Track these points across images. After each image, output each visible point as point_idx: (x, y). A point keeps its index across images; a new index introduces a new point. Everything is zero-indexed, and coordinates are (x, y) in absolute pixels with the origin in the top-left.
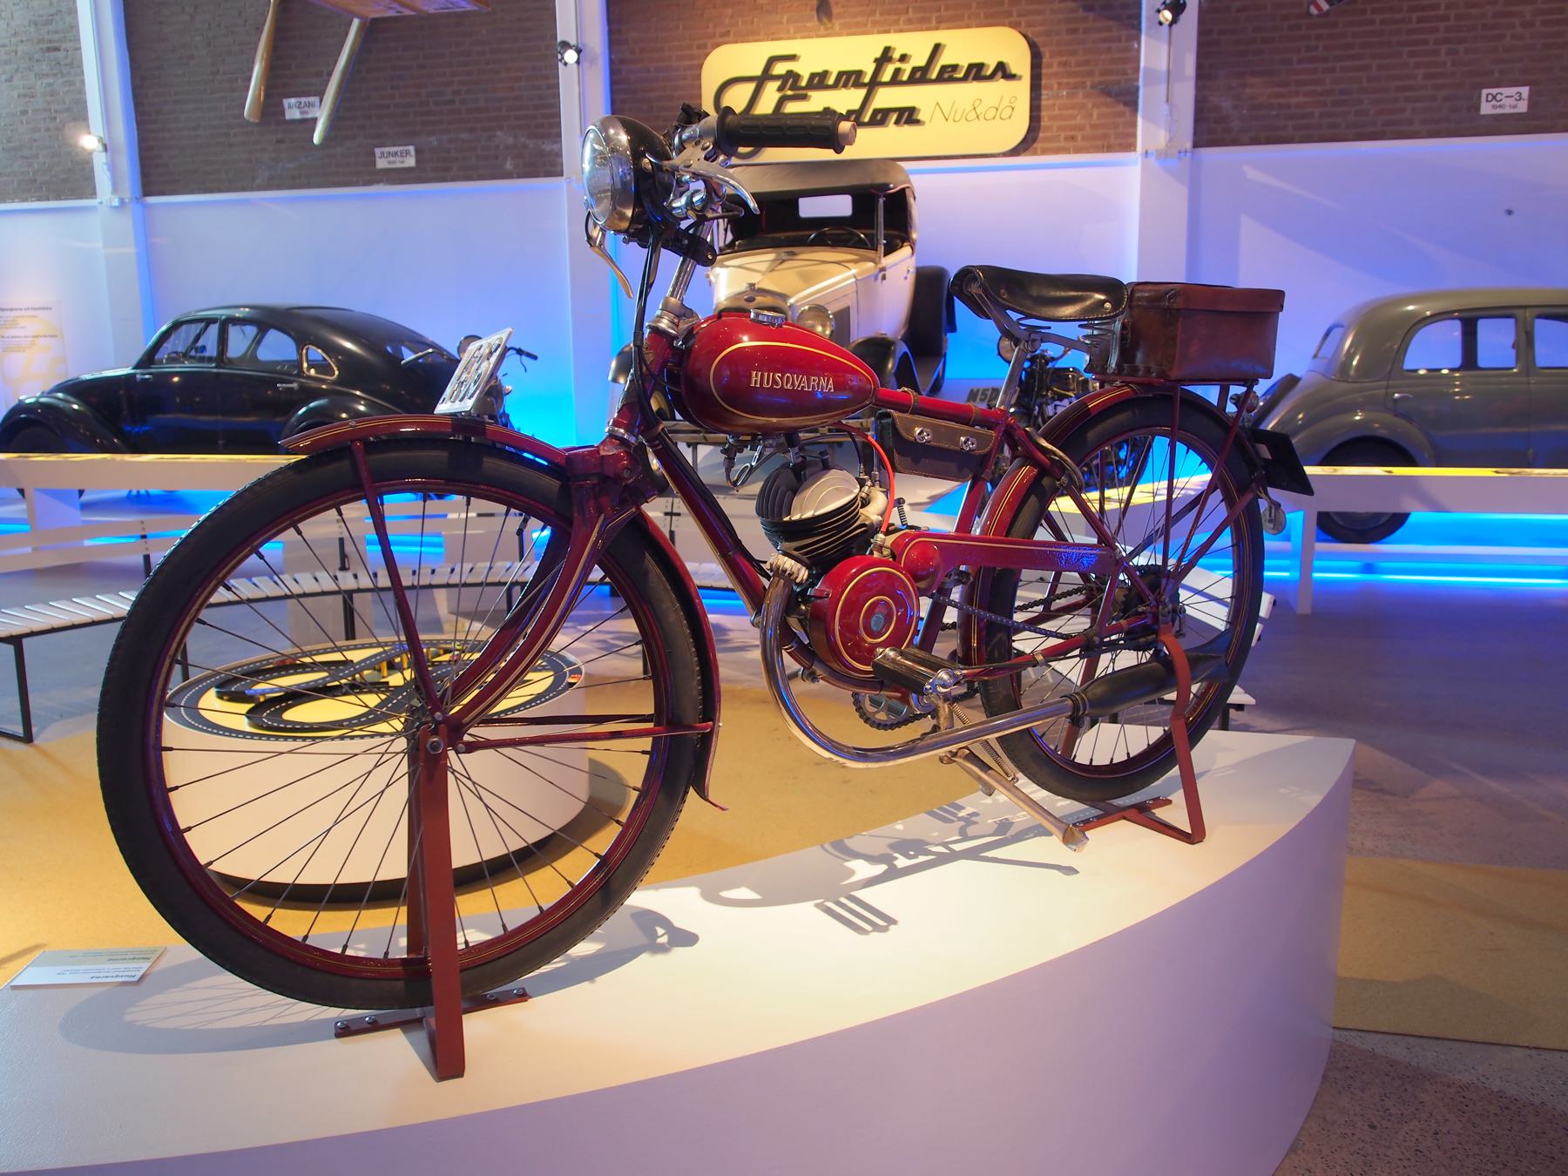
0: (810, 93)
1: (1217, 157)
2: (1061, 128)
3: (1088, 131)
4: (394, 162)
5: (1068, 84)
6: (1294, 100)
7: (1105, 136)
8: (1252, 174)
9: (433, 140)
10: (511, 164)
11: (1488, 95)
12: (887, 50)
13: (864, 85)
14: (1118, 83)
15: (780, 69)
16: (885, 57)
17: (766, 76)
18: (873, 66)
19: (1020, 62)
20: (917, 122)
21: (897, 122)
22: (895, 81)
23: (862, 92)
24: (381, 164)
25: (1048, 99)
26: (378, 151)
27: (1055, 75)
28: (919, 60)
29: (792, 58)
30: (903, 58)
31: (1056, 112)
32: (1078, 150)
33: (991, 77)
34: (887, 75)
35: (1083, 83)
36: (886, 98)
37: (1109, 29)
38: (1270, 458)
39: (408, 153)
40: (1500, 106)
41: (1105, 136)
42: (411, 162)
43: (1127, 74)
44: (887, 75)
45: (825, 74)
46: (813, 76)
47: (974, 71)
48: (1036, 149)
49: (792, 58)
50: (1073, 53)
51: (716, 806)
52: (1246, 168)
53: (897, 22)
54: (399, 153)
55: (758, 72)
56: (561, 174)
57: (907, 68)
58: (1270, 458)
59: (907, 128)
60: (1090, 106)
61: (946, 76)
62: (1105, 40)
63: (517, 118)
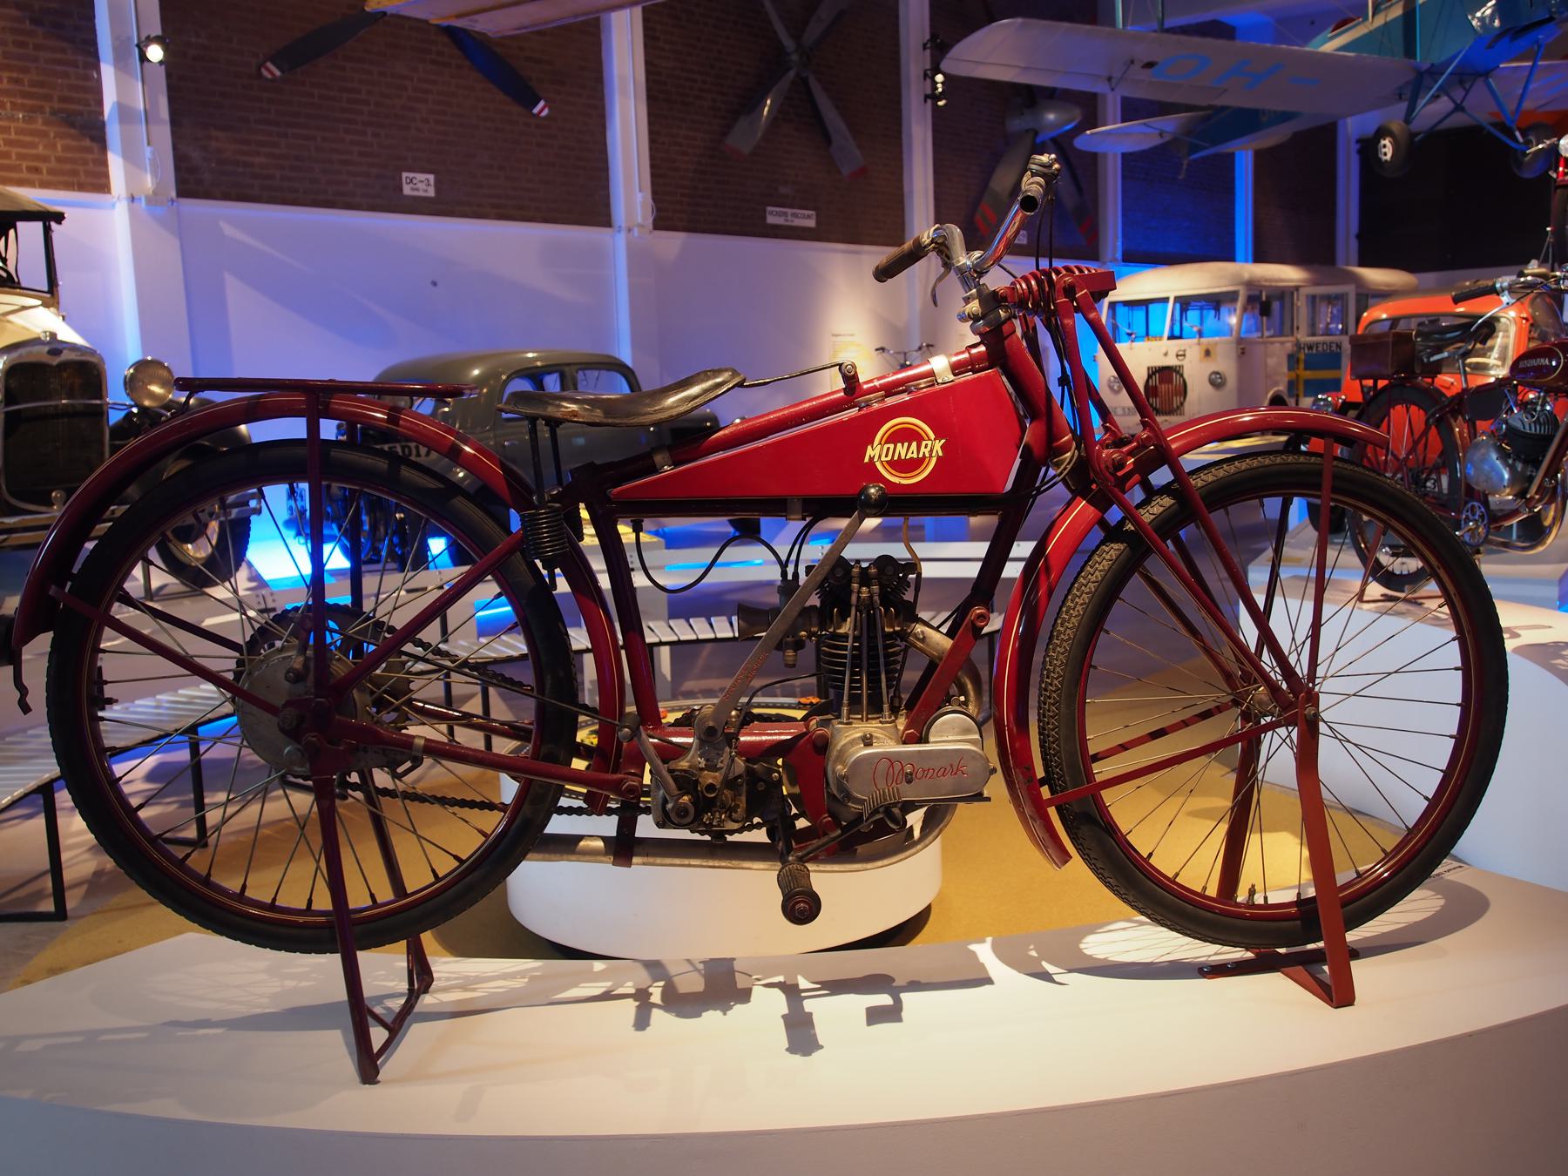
1: (200, 209)
3: (53, 164)
6: (257, 160)
7: (74, 173)
8: (228, 230)
11: (406, 178)
14: (81, 113)
43: (89, 106)
50: (25, 70)
60: (52, 135)
62: (59, 62)
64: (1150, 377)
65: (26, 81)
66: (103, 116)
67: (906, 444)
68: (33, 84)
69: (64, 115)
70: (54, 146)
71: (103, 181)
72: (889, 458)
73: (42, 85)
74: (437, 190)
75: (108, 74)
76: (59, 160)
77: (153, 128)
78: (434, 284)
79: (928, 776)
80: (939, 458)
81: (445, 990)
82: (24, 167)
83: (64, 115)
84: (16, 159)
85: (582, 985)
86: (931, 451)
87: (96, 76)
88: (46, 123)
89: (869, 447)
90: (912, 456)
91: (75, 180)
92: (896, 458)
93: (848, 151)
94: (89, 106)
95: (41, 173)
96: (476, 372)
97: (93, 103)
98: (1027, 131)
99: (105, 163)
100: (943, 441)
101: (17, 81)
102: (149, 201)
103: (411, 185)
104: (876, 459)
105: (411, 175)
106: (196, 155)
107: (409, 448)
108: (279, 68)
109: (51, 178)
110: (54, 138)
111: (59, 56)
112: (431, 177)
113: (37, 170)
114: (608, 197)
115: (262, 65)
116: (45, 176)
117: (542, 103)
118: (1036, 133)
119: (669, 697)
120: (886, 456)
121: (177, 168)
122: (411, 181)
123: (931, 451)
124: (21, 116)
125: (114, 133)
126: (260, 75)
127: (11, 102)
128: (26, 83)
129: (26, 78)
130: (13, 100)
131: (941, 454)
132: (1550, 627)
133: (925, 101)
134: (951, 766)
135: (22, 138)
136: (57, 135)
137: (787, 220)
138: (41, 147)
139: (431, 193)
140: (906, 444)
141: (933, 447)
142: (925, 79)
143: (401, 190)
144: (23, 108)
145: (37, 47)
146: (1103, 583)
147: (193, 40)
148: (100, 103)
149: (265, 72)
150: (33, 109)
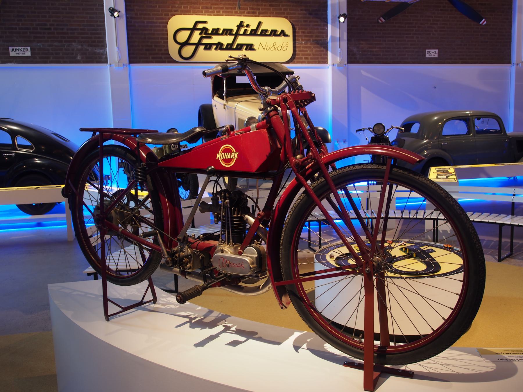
3: (312, 56)
6: (375, 50)
7: (318, 58)
8: (364, 73)
11: (427, 51)
40: (431, 55)
42: (28, 54)
50: (306, 29)
52: (362, 71)
54: (22, 50)
60: (312, 47)
62: (316, 25)
65: (306, 32)
66: (327, 40)
67: (227, 153)
69: (316, 41)
70: (313, 50)
71: (326, 60)
72: (223, 158)
73: (310, 33)
74: (438, 55)
75: (329, 26)
76: (314, 55)
77: (342, 43)
78: (435, 88)
79: (237, 265)
80: (236, 158)
81: (159, 304)
82: (303, 57)
83: (316, 41)
84: (302, 56)
85: (187, 312)
86: (234, 156)
87: (326, 28)
88: (311, 44)
89: (218, 154)
90: (229, 158)
92: (225, 158)
94: (324, 37)
95: (308, 59)
97: (325, 37)
99: (327, 55)
100: (238, 153)
101: (303, 32)
103: (429, 54)
104: (219, 158)
105: (429, 50)
106: (355, 50)
108: (384, 19)
109: (311, 60)
110: (313, 48)
111: (316, 23)
112: (437, 51)
113: (307, 58)
114: (510, 52)
115: (379, 18)
116: (309, 60)
117: (484, 20)
119: (515, 227)
120: (222, 157)
121: (348, 54)
122: (429, 52)
123: (234, 156)
124: (304, 43)
126: (378, 22)
127: (301, 39)
128: (306, 33)
129: (306, 31)
130: (302, 38)
131: (237, 158)
132: (119, 244)
134: (240, 264)
135: (304, 49)
136: (314, 47)
138: (309, 51)
139: (436, 56)
140: (227, 153)
141: (235, 155)
143: (425, 55)
144: (305, 40)
145: (310, 22)
146: (297, 207)
147: (357, 13)
148: (327, 36)
149: (380, 21)
150: (307, 41)
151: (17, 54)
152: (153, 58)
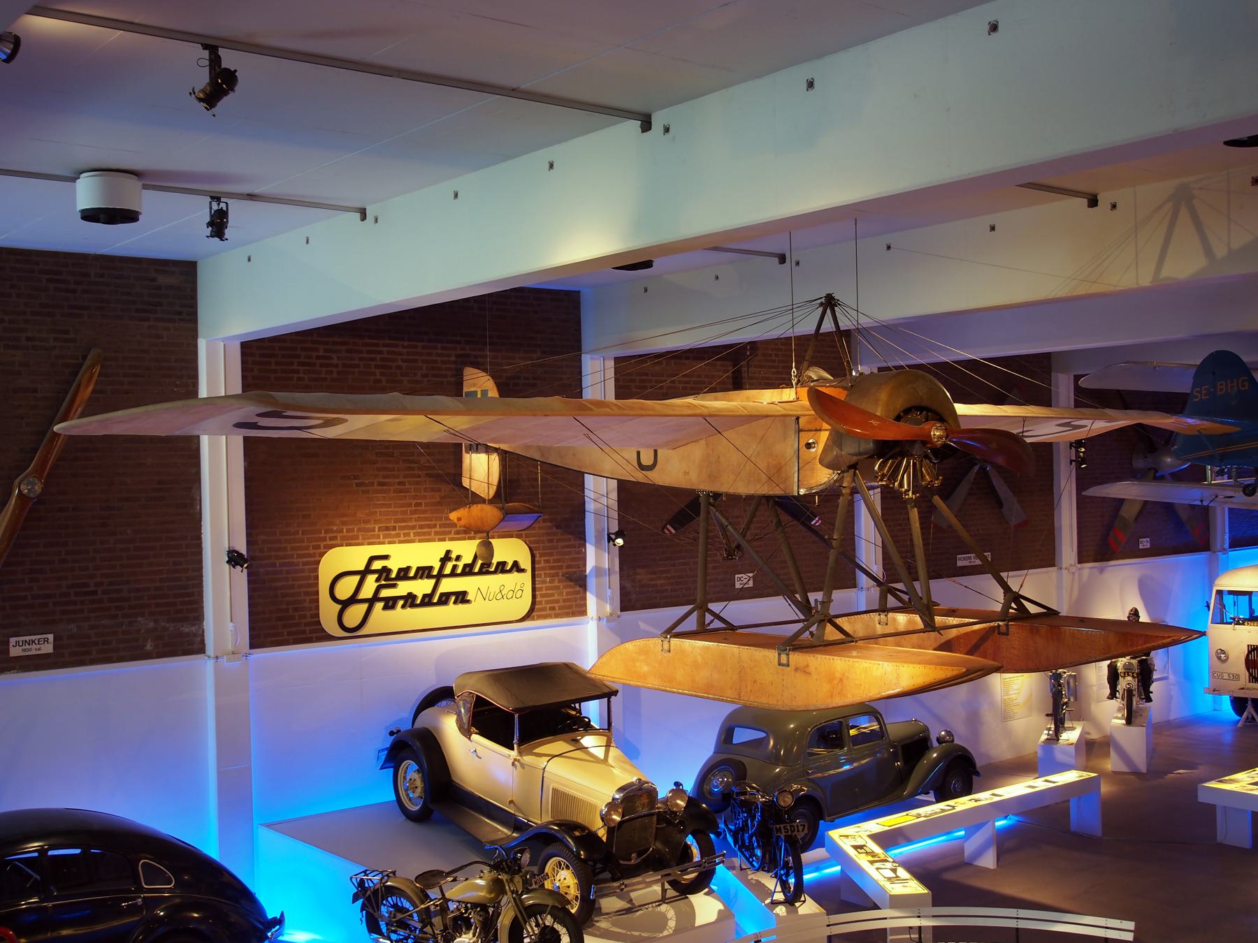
0: (399, 583)
1: (630, 615)
2: (547, 602)
3: (561, 604)
4: (29, 650)
5: (550, 574)
6: (659, 582)
7: (570, 607)
9: (73, 628)
10: (151, 646)
12: (448, 552)
13: (433, 577)
14: (575, 573)
15: (377, 565)
16: (446, 558)
17: (364, 574)
18: (439, 564)
19: (526, 563)
20: (468, 602)
21: (455, 602)
22: (453, 574)
23: (433, 581)
24: (15, 652)
25: (539, 584)
26: (13, 640)
27: (544, 569)
28: (468, 559)
29: (386, 557)
30: (458, 558)
31: (544, 592)
32: (557, 616)
33: (510, 571)
34: (448, 570)
35: (558, 573)
36: (448, 585)
37: (569, 540)
38: (605, 841)
39: (46, 640)
41: (570, 607)
42: (48, 648)
43: (579, 568)
44: (448, 570)
45: (408, 568)
46: (400, 570)
47: (500, 567)
48: (534, 616)
49: (386, 557)
50: (551, 555)
51: (886, 918)
52: (640, 623)
53: (450, 533)
54: (36, 642)
55: (362, 568)
56: (201, 650)
57: (461, 565)
58: (605, 841)
59: (460, 606)
60: (562, 587)
61: (484, 570)
62: (567, 547)
63: (157, 605)
64: (1249, 652)
68: (555, 561)
75: (591, 551)
91: (571, 610)
93: (1014, 511)
96: (792, 726)
98: (1149, 469)
99: (585, 599)
102: (608, 620)
107: (793, 826)
109: (560, 611)
115: (665, 527)
118: (1156, 471)
125: (592, 582)
133: (1071, 464)
137: (970, 562)
142: (1071, 448)
151: (24, 650)
152: (289, 634)
